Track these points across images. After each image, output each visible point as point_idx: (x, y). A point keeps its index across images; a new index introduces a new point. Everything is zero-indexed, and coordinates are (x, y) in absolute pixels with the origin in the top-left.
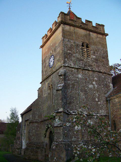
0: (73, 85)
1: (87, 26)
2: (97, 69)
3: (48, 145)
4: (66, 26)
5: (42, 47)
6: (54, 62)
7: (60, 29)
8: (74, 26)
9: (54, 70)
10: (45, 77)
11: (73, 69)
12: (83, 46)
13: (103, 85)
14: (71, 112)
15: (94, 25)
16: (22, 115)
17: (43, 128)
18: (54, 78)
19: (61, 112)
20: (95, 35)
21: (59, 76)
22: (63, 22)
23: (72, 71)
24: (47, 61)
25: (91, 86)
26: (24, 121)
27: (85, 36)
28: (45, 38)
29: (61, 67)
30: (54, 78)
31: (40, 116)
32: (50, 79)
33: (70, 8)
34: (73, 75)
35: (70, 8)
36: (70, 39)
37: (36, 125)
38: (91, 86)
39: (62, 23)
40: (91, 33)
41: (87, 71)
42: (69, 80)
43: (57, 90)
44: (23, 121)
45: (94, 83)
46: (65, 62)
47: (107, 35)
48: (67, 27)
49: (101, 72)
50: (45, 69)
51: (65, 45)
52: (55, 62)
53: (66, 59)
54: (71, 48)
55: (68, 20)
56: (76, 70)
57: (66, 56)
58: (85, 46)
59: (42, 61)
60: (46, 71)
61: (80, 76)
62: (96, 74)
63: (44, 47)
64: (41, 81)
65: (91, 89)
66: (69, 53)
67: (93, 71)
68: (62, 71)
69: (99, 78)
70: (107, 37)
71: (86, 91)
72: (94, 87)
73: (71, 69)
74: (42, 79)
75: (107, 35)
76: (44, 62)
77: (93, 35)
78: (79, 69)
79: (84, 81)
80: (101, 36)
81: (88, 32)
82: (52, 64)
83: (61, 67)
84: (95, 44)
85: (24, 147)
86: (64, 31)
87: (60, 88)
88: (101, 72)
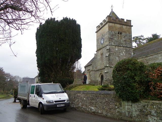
0: (113, 54)
1: (121, 22)
2: (125, 46)
3: (101, 81)
4: (110, 23)
5: (97, 32)
6: (103, 42)
7: (107, 26)
8: (115, 23)
9: (104, 46)
10: (98, 49)
11: (113, 46)
12: (118, 33)
13: (128, 53)
14: (112, 66)
15: (125, 21)
16: (85, 67)
17: (98, 74)
18: (104, 51)
19: (107, 66)
20: (125, 27)
21: (107, 50)
22: (109, 22)
23: (113, 47)
24: (100, 41)
25: (122, 54)
26: (86, 70)
27: (120, 28)
28: (98, 27)
29: (108, 45)
30: (104, 51)
31: (96, 68)
32: (101, 50)
33: (112, 10)
34: (113, 49)
35: (112, 10)
36: (112, 31)
37: (94, 72)
38: (122, 54)
39: (108, 22)
40: (123, 26)
41: (120, 47)
42: (111, 51)
43: (106, 57)
44: (86, 70)
45: (123, 53)
46: (109, 43)
47: (132, 26)
48: (111, 24)
49: (127, 47)
50: (99, 44)
51: (110, 34)
52: (104, 42)
53: (110, 41)
54: (112, 35)
55: (112, 19)
56: (115, 47)
57: (111, 39)
58: (120, 34)
59: (97, 40)
60: (99, 46)
61: (116, 49)
62: (124, 48)
63: (98, 33)
64: (96, 50)
65: (122, 55)
66: (112, 38)
67: (123, 47)
68: (108, 47)
69: (126, 50)
70: (132, 27)
71: (119, 56)
72: (123, 55)
73: (112, 46)
74: (97, 50)
75: (132, 26)
76: (97, 40)
77: (124, 27)
78: (117, 46)
79: (118, 52)
80: (129, 27)
81: (122, 26)
82: (102, 42)
83: (108, 45)
84: (125, 32)
85: (138, 60)
86: (110, 27)
87: (107, 56)
88: (127, 47)
